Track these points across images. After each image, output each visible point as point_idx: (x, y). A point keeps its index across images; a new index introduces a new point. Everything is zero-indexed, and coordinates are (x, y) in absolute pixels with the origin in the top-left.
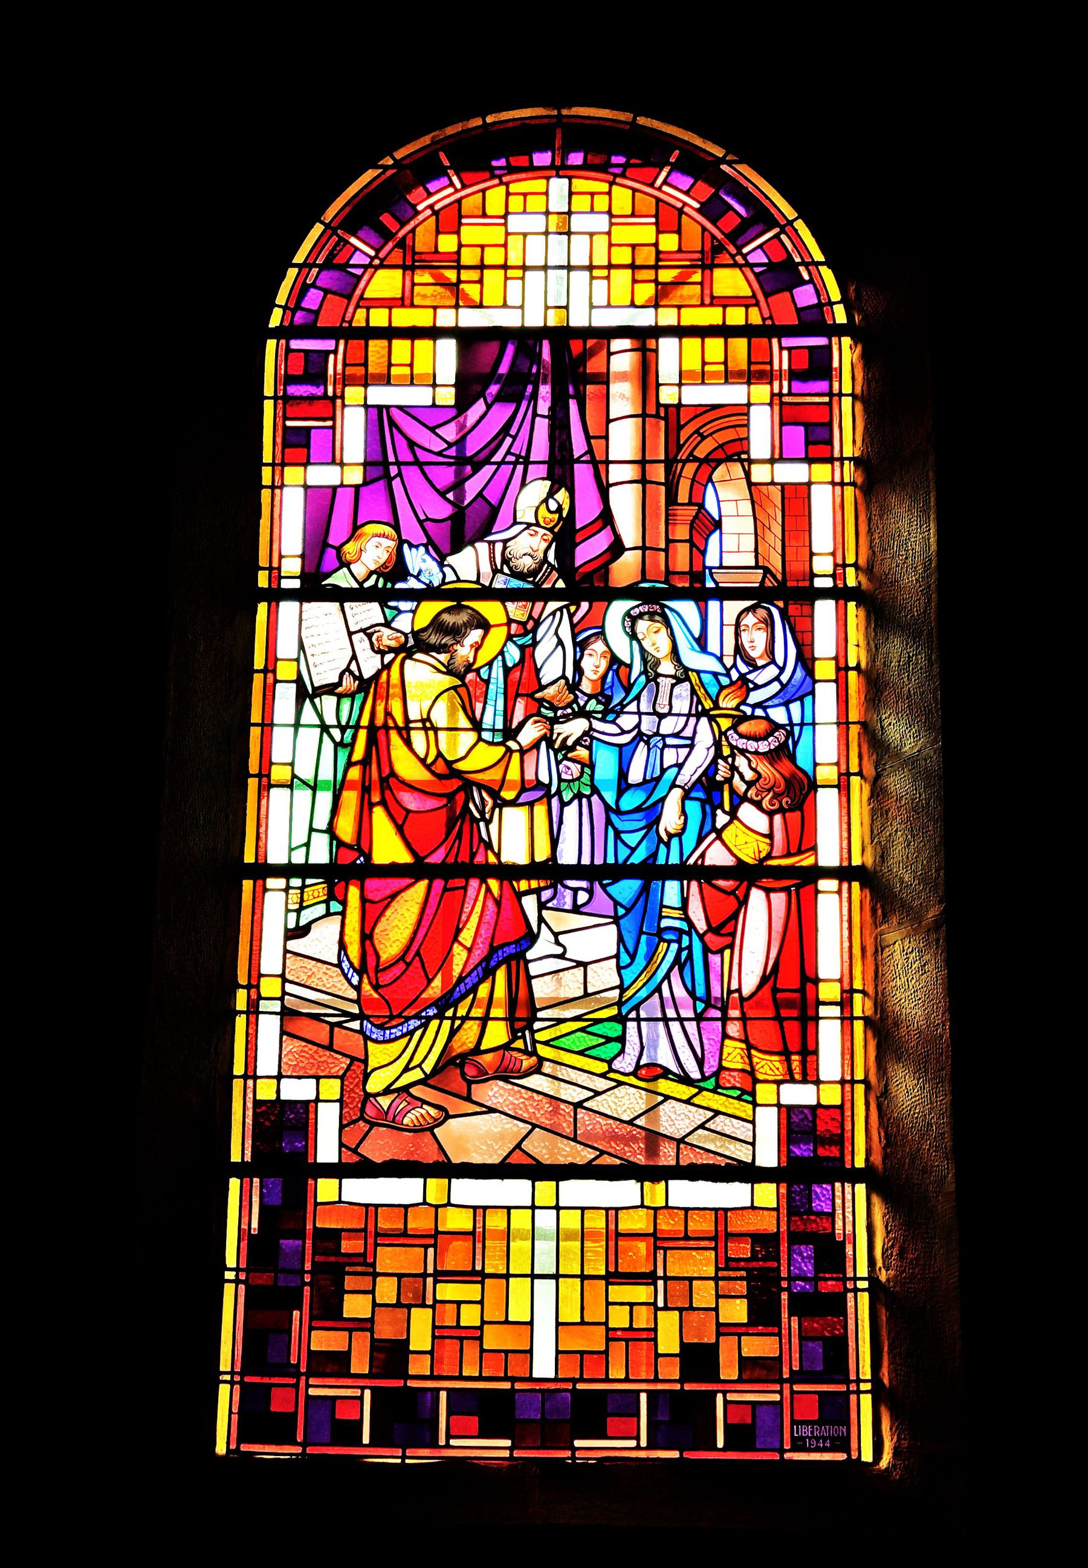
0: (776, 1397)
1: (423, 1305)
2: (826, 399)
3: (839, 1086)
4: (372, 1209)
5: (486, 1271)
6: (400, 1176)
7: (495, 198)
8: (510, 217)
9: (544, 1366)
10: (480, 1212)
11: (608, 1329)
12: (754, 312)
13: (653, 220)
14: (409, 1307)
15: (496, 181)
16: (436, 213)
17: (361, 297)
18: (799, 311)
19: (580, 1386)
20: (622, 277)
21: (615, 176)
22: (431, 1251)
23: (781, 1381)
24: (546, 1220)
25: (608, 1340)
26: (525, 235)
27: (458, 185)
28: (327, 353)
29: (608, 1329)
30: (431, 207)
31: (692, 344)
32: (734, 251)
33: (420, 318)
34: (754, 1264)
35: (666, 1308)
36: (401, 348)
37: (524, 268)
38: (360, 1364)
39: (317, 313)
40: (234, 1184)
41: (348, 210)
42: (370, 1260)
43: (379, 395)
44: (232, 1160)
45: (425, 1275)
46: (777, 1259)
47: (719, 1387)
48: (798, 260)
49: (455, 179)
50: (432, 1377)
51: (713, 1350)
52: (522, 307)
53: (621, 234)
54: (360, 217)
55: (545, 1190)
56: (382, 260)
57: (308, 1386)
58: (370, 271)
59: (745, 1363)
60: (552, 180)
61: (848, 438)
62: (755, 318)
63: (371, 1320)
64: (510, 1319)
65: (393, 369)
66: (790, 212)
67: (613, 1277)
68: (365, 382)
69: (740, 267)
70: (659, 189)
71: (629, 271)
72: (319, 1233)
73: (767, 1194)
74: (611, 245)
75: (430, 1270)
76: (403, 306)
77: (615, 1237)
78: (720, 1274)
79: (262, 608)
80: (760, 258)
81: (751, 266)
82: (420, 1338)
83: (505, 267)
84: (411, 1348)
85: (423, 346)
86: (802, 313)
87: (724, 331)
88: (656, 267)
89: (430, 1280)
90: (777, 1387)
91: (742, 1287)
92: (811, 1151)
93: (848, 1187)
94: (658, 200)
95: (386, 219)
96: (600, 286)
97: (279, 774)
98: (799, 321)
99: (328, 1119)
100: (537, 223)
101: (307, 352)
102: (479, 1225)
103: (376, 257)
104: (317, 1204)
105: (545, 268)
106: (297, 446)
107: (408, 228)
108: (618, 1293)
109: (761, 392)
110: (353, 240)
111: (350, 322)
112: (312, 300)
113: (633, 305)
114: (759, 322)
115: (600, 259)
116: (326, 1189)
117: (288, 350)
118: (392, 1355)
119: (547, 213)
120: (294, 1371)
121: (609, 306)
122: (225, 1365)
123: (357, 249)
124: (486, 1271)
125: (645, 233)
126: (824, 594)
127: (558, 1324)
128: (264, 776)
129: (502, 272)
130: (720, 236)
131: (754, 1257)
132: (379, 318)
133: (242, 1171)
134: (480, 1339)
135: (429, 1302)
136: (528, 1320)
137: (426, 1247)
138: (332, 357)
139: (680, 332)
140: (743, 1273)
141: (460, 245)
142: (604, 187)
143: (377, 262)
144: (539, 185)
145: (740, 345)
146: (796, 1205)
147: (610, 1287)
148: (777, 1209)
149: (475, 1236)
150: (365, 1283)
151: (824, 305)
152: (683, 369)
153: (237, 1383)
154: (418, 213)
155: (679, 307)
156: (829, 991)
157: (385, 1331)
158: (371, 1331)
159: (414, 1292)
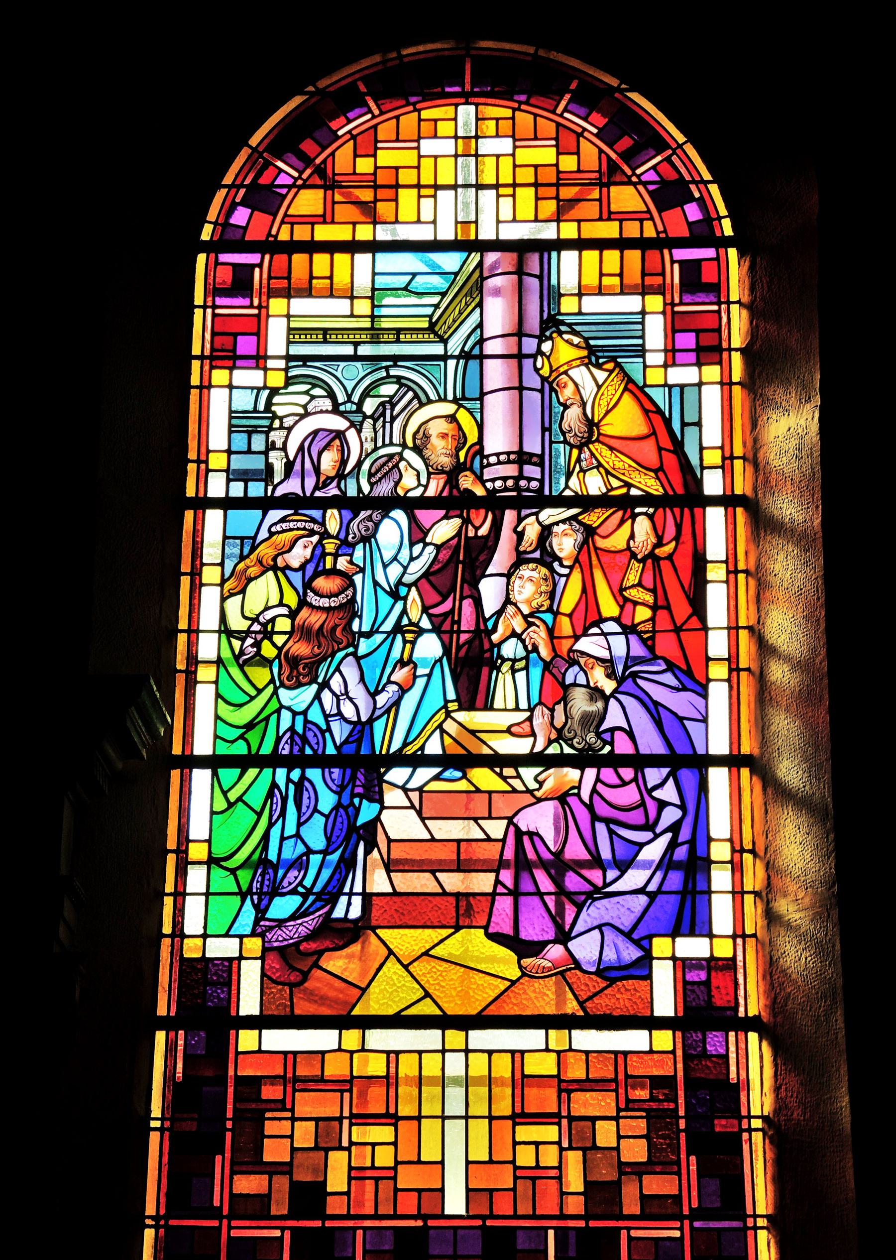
0: (677, 1234)
1: (340, 1148)
2: (715, 308)
3: (730, 941)
4: (290, 1056)
5: (400, 1114)
6: (315, 1029)
7: (409, 121)
8: (422, 141)
9: (455, 1203)
10: (392, 1056)
11: (516, 1168)
12: (648, 226)
13: (553, 142)
14: (327, 1150)
15: (411, 108)
16: (354, 138)
17: (286, 215)
18: (690, 225)
19: (489, 1223)
20: (526, 195)
21: (520, 103)
22: (347, 1095)
23: (680, 1217)
24: (455, 1065)
25: (516, 1178)
26: (436, 157)
27: (377, 112)
28: (253, 266)
29: (516, 1168)
30: (349, 132)
31: (591, 256)
32: (629, 172)
33: (341, 233)
34: (654, 1105)
35: (570, 1148)
36: (321, 261)
37: (437, 187)
38: (280, 1207)
39: (245, 229)
40: (160, 1037)
41: (271, 137)
42: (289, 1106)
43: (300, 305)
44: (174, 753)
45: (340, 1119)
46: (675, 1101)
47: (620, 1224)
48: (687, 177)
49: (372, 104)
50: (348, 1217)
51: (615, 1188)
52: (434, 222)
53: (526, 156)
54: (284, 143)
55: (455, 1038)
56: (305, 181)
57: (230, 1228)
58: (294, 190)
59: (644, 1198)
60: (460, 108)
61: (737, 327)
62: (650, 231)
63: (290, 1164)
64: (422, 1159)
65: (314, 281)
66: (681, 138)
67: (519, 1117)
68: (288, 293)
69: (634, 185)
70: (561, 116)
71: (533, 189)
72: (239, 1080)
73: (664, 1040)
74: (515, 166)
75: (346, 1113)
76: (324, 222)
77: (522, 1081)
78: (622, 1114)
79: (175, 775)
80: (652, 176)
81: (645, 184)
82: (337, 1181)
83: (418, 186)
84: (329, 1190)
85: (342, 259)
86: (693, 226)
87: (621, 244)
88: (557, 185)
89: (346, 1123)
90: (678, 1225)
91: (641, 1126)
92: (705, 1008)
93: (741, 1036)
94: (558, 125)
95: (308, 146)
96: (506, 204)
97: (197, 852)
98: (691, 232)
99: (250, 976)
100: (447, 147)
101: (234, 265)
102: (392, 1070)
103: (300, 177)
104: (238, 1053)
105: (454, 187)
106: (225, 355)
107: (329, 151)
108: (525, 1133)
109: (655, 302)
110: (279, 164)
111: (276, 236)
112: (240, 217)
113: (536, 220)
114: (654, 235)
115: (506, 177)
116: (247, 1040)
117: (217, 263)
118: (310, 1196)
119: (456, 137)
120: (216, 1214)
121: (514, 220)
122: (150, 1209)
123: (281, 170)
124: (400, 1114)
125: (547, 155)
126: (715, 501)
127: (468, 1163)
128: (203, 462)
129: (416, 190)
130: (613, 156)
131: (652, 1099)
132: (302, 233)
133: (167, 1024)
134: (395, 1179)
135: (345, 1143)
136: (440, 1159)
137: (342, 1092)
138: (257, 270)
139: (580, 244)
140: (644, 1114)
141: (376, 168)
142: (508, 113)
143: (300, 182)
144: (449, 111)
145: (634, 256)
146: (694, 1055)
147: (517, 1127)
148: (673, 1052)
149: (390, 1081)
150: (284, 1127)
151: (709, 220)
152: (583, 283)
153: (162, 1227)
154: (339, 137)
155: (579, 221)
156: (720, 851)
157: (302, 1176)
158: (290, 1173)
159: (328, 1137)
